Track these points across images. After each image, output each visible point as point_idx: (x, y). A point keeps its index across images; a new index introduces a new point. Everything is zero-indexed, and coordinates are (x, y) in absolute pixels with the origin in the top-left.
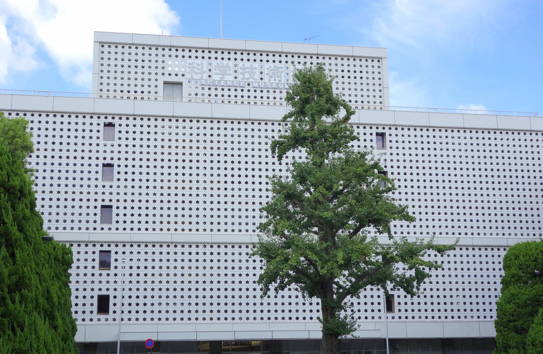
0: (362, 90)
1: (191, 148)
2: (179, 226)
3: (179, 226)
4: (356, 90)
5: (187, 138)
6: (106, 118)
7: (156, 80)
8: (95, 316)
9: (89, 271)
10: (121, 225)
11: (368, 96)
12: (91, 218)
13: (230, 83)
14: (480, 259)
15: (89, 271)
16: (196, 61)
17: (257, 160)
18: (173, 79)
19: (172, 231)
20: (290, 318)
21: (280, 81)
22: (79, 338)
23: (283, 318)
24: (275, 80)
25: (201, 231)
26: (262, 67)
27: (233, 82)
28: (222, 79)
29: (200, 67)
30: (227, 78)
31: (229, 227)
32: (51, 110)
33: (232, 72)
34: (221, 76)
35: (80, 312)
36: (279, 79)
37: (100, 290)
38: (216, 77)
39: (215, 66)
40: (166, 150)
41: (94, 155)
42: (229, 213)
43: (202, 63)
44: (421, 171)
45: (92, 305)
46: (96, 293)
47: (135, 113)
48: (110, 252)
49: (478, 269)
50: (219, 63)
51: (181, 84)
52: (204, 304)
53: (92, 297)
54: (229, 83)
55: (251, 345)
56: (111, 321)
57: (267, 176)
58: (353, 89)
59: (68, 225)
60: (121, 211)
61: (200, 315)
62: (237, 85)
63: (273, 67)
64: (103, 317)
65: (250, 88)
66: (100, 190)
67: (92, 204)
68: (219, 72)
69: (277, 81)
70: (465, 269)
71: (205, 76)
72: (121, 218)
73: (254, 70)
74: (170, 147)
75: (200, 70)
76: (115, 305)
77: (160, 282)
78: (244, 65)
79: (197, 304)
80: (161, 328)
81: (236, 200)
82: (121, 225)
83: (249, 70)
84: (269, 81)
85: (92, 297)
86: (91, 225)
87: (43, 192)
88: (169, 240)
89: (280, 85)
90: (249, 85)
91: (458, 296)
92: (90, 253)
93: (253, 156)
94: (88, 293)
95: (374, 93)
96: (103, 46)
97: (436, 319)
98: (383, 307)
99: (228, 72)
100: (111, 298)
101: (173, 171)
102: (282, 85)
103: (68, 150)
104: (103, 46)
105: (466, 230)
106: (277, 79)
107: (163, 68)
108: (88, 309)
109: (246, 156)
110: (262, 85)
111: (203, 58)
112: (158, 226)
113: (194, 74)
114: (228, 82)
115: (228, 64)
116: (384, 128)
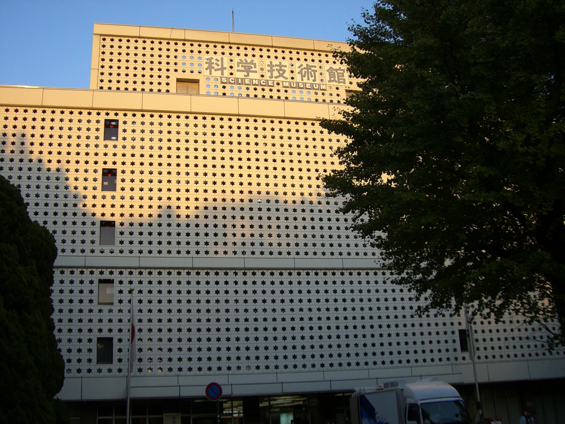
4: (293, 186)
5: (209, 138)
6: (107, 114)
8: (94, 366)
10: (126, 247)
12: (88, 237)
14: (354, 323)
16: (215, 57)
17: (296, 166)
18: (188, 76)
20: (392, 362)
21: (314, 80)
22: (95, 25)
23: (340, 365)
24: (308, 79)
34: (246, 73)
35: (65, 331)
38: (241, 75)
40: (183, 153)
43: (222, 59)
47: (144, 108)
48: (115, 190)
49: (367, 327)
50: (243, 59)
51: (197, 81)
54: (254, 82)
56: (115, 372)
64: (105, 367)
68: (243, 69)
69: (312, 82)
70: (367, 327)
71: (226, 73)
73: (283, 68)
74: (141, 243)
76: (120, 350)
78: (271, 62)
80: (183, 381)
82: (126, 247)
83: (278, 68)
84: (302, 80)
85: (90, 340)
89: (314, 85)
90: (278, 84)
94: (85, 336)
98: (458, 345)
99: (253, 69)
100: (115, 341)
101: (201, 169)
102: (317, 85)
103: (59, 153)
108: (84, 356)
109: (249, 159)
110: (294, 85)
111: (223, 54)
115: (252, 61)
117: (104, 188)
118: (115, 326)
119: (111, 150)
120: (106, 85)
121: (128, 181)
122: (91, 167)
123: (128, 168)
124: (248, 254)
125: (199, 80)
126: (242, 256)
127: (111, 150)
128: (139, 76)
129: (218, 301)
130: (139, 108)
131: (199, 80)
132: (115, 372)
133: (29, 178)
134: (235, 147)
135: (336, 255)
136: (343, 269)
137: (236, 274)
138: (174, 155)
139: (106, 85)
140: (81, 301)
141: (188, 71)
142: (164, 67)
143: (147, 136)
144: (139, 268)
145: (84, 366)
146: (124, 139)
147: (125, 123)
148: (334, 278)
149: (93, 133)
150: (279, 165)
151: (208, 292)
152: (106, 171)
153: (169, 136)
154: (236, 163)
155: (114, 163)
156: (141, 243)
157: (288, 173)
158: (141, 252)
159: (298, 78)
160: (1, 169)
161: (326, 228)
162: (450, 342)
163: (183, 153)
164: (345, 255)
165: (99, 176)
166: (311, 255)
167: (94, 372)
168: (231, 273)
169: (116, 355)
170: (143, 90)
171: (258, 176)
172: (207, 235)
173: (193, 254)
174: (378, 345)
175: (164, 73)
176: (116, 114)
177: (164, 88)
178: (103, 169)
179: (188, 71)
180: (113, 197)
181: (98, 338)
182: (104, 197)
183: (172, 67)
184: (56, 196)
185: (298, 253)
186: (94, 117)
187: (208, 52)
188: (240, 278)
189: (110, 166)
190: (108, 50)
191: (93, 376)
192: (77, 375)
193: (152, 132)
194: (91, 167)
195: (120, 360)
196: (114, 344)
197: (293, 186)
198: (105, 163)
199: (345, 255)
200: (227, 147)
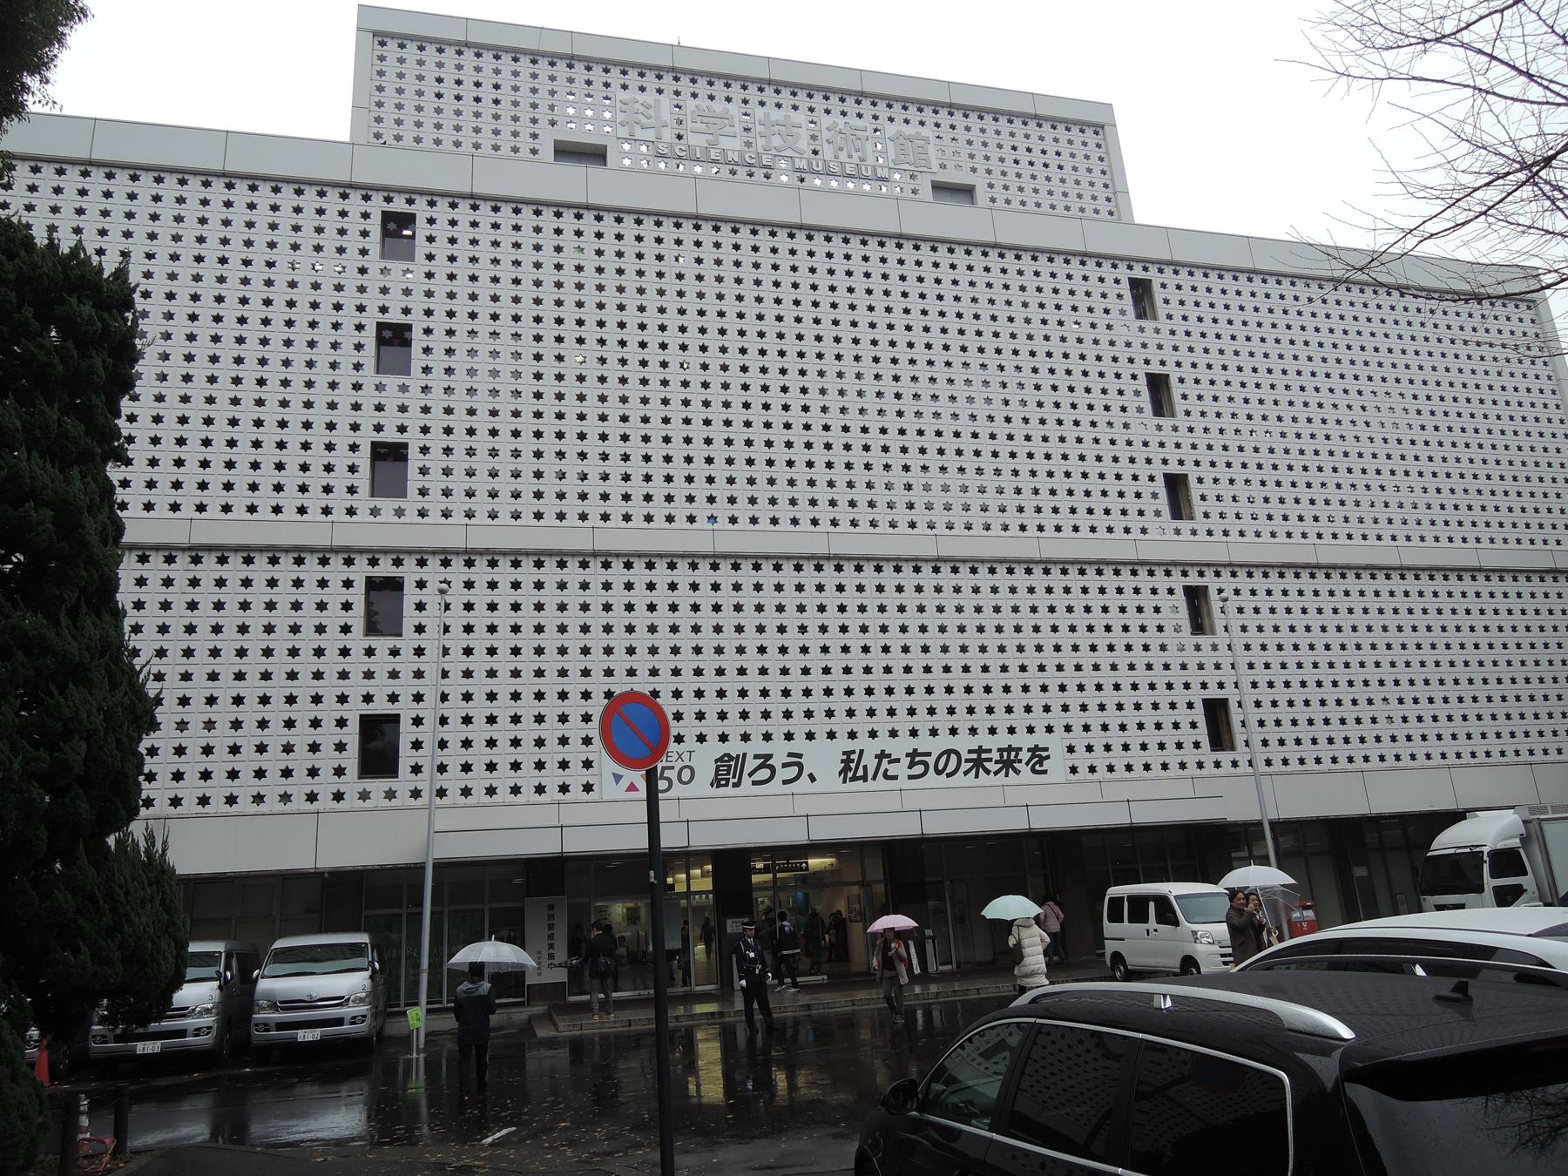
0: (813, 502)
1: (539, 651)
6: (373, 562)
8: (352, 783)
27: (741, 153)
28: (712, 145)
29: (651, 112)
30: (725, 143)
32: (216, 166)
33: (738, 129)
34: (710, 137)
36: (860, 154)
37: (368, 698)
39: (692, 112)
41: (330, 687)
44: (797, 704)
46: (354, 711)
48: (408, 373)
52: (722, 716)
53: (341, 723)
54: (730, 156)
55: (807, 868)
56: (404, 798)
60: (427, 733)
62: (753, 161)
63: (841, 126)
64: (378, 786)
75: (652, 120)
85: (341, 723)
87: (318, 675)
88: (587, 546)
95: (757, 598)
96: (382, 44)
97: (1343, 763)
98: (1202, 734)
99: (728, 130)
100: (405, 724)
106: (856, 155)
107: (552, 108)
111: (660, 91)
113: (637, 127)
114: (730, 153)
116: (1145, 269)
117: (372, 629)
119: (381, 664)
124: (723, 522)
126: (709, 526)
127: (381, 664)
130: (467, 189)
132: (404, 798)
133: (243, 629)
135: (922, 528)
136: (938, 559)
144: (466, 551)
145: (325, 784)
147: (428, 331)
152: (387, 334)
155: (406, 311)
159: (827, 152)
161: (730, 651)
162: (1185, 726)
164: (941, 529)
165: (363, 459)
166: (864, 526)
167: (351, 801)
173: (594, 519)
182: (370, 652)
185: (834, 523)
186: (355, 204)
187: (625, 87)
188: (704, 575)
189: (395, 317)
191: (348, 809)
192: (308, 806)
195: (420, 629)
197: (789, 445)
198: (368, 698)
199: (941, 529)
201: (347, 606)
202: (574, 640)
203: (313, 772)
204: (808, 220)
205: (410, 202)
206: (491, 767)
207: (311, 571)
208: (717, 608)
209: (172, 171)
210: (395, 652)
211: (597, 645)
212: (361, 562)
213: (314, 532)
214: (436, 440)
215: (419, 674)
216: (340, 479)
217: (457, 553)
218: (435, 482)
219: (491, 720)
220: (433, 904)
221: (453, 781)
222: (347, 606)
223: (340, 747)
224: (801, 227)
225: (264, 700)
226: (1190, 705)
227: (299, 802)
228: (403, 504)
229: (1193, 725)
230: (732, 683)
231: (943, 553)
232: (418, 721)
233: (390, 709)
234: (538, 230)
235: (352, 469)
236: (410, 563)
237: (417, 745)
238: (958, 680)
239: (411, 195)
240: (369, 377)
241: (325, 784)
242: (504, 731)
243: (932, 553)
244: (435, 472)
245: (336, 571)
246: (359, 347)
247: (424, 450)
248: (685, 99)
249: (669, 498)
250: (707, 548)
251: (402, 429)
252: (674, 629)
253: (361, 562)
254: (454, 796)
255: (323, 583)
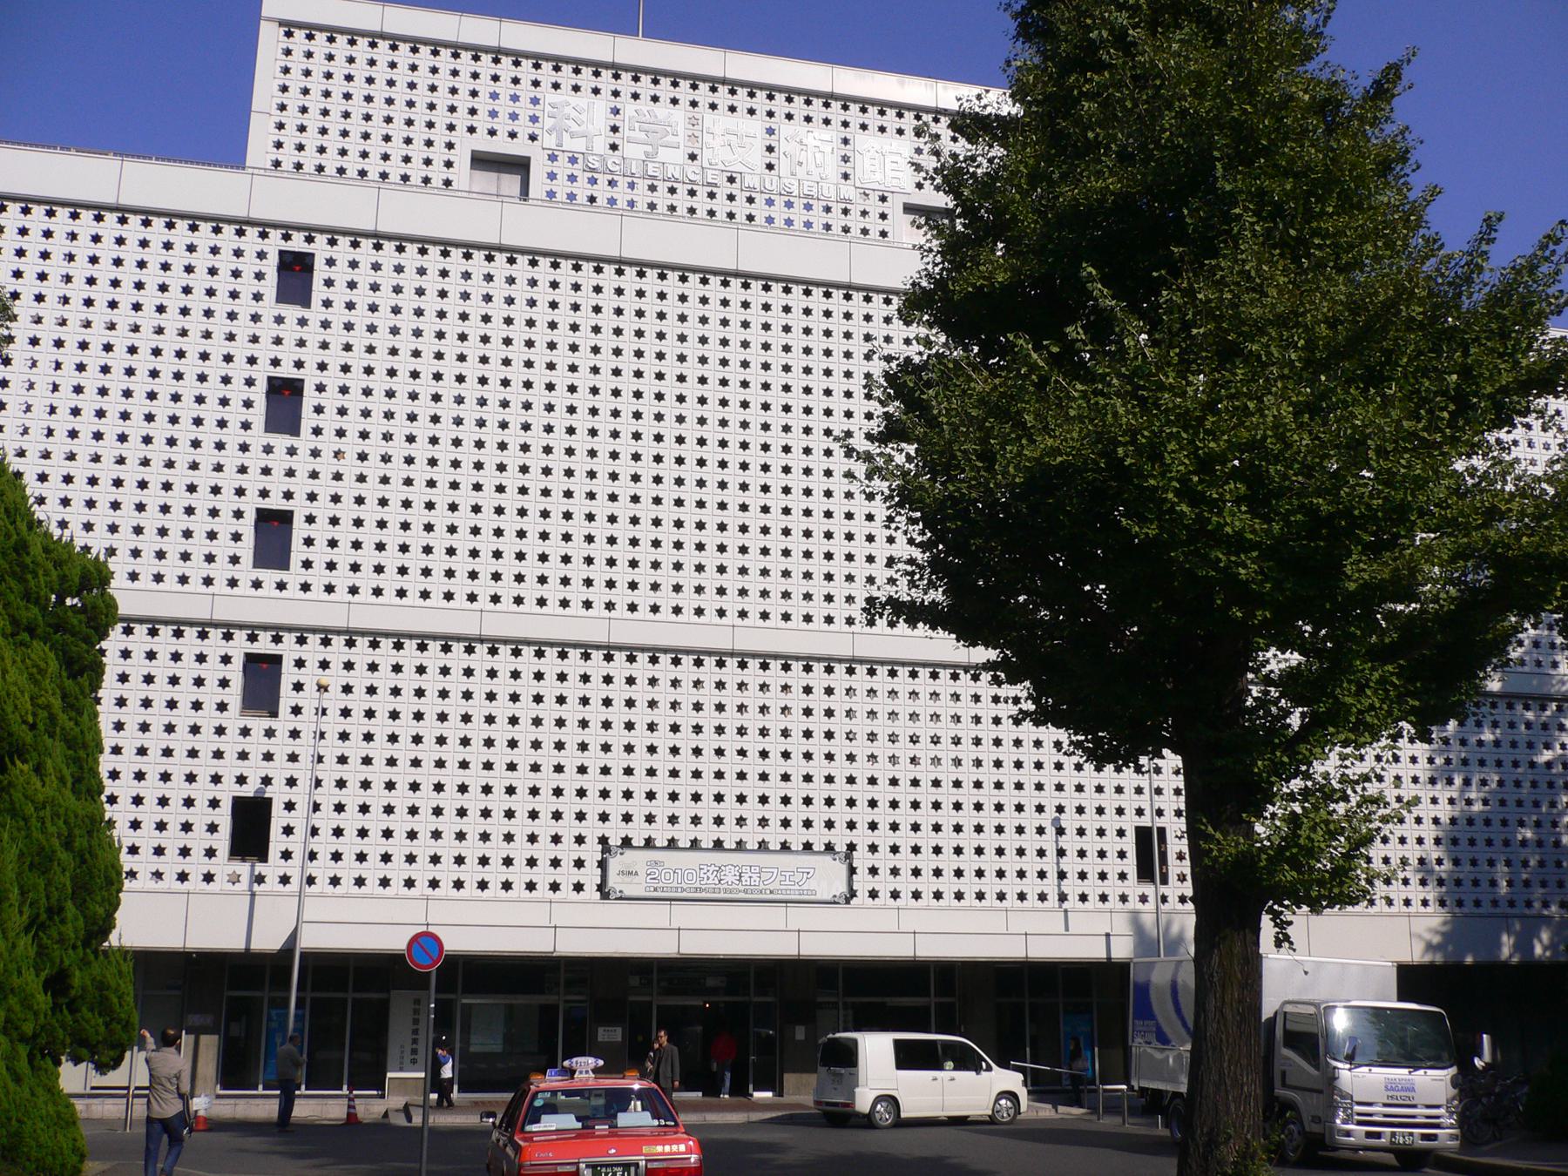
2: (530, 590)
3: (507, 589)
4: (744, 487)
6: (287, 237)
7: (450, 146)
8: (223, 865)
9: (208, 718)
10: (319, 576)
11: (680, 461)
13: (672, 171)
15: (208, 718)
16: (575, 99)
19: (484, 601)
25: (576, 608)
26: (694, 122)
29: (584, 117)
30: (664, 155)
31: (666, 599)
32: (110, 199)
34: (649, 149)
41: (205, 767)
42: (667, 555)
45: (213, 828)
46: (227, 792)
50: (645, 109)
57: (828, 432)
58: (713, 422)
59: (437, 584)
60: (322, 531)
61: (447, 872)
64: (270, 577)
65: (734, 189)
66: (255, 459)
67: (227, 503)
68: (642, 135)
71: (601, 146)
72: (320, 554)
76: (298, 687)
77: (440, 764)
79: (555, 863)
81: (690, 514)
82: (319, 576)
86: (221, 571)
91: (893, 713)
92: (213, 659)
93: (745, 384)
98: (1130, 865)
99: (670, 138)
104: (289, 34)
105: (785, 606)
112: (553, 592)
118: (279, 770)
120: (288, 157)
121: (340, 284)
122: (202, 791)
123: (333, 378)
125: (528, 159)
127: (279, 461)
128: (376, 138)
129: (537, 722)
131: (528, 159)
134: (607, 341)
137: (586, 656)
138: (441, 523)
139: (288, 157)
140: (197, 706)
141: (502, 134)
142: (441, 117)
143: (384, 320)
145: (196, 865)
146: (327, 304)
148: (828, 681)
149: (235, 414)
150: (712, 453)
151: (520, 556)
153: (438, 366)
154: (606, 382)
156: (357, 545)
157: (733, 476)
158: (354, 590)
160: (3, 384)
163: (466, 476)
168: (574, 654)
169: (277, 842)
170: (384, 176)
171: (660, 376)
172: (520, 578)
174: (926, 806)
175: (440, 135)
176: (277, 639)
177: (437, 173)
178: (270, 379)
179: (502, 134)
180: (292, 451)
181: (247, 655)
183: (462, 119)
184: (140, 507)
190: (297, 63)
193: (389, 415)
194: (202, 791)
195: (296, 710)
196: (304, 415)
198: (276, 362)
200: (582, 421)
201: (224, 683)
202: (468, 454)
203: (195, 730)
204: (745, 267)
205: (310, 240)
206: (361, 857)
207: (190, 644)
208: (612, 519)
209: (64, 204)
210: (270, 733)
211: (487, 527)
212: (240, 636)
213: (193, 605)
214: (333, 378)
215: (293, 758)
216: (247, 286)
217: (339, 632)
218: (340, 294)
219: (380, 547)
220: (298, 990)
221: (322, 869)
222: (237, 537)
223: (224, 683)
224: (737, 275)
225: (138, 801)
226: (1121, 833)
227: (170, 881)
228: (260, 868)
229: (1122, 855)
230: (646, 511)
231: (859, 653)
232: (321, 388)
233: (283, 505)
234: (455, 73)
235: (237, 537)
236: (289, 639)
237: (329, 283)
238: (862, 792)
239: (310, 233)
240: (269, 308)
241: (196, 865)
242: (393, 536)
243: (846, 652)
244: (331, 411)
245: (215, 645)
246: (248, 404)
247: (321, 388)
248: (625, 102)
249: (572, 410)
250: (601, 638)
251: (288, 495)
252: (572, 410)
253: (240, 636)
254: (322, 884)
255: (201, 658)
